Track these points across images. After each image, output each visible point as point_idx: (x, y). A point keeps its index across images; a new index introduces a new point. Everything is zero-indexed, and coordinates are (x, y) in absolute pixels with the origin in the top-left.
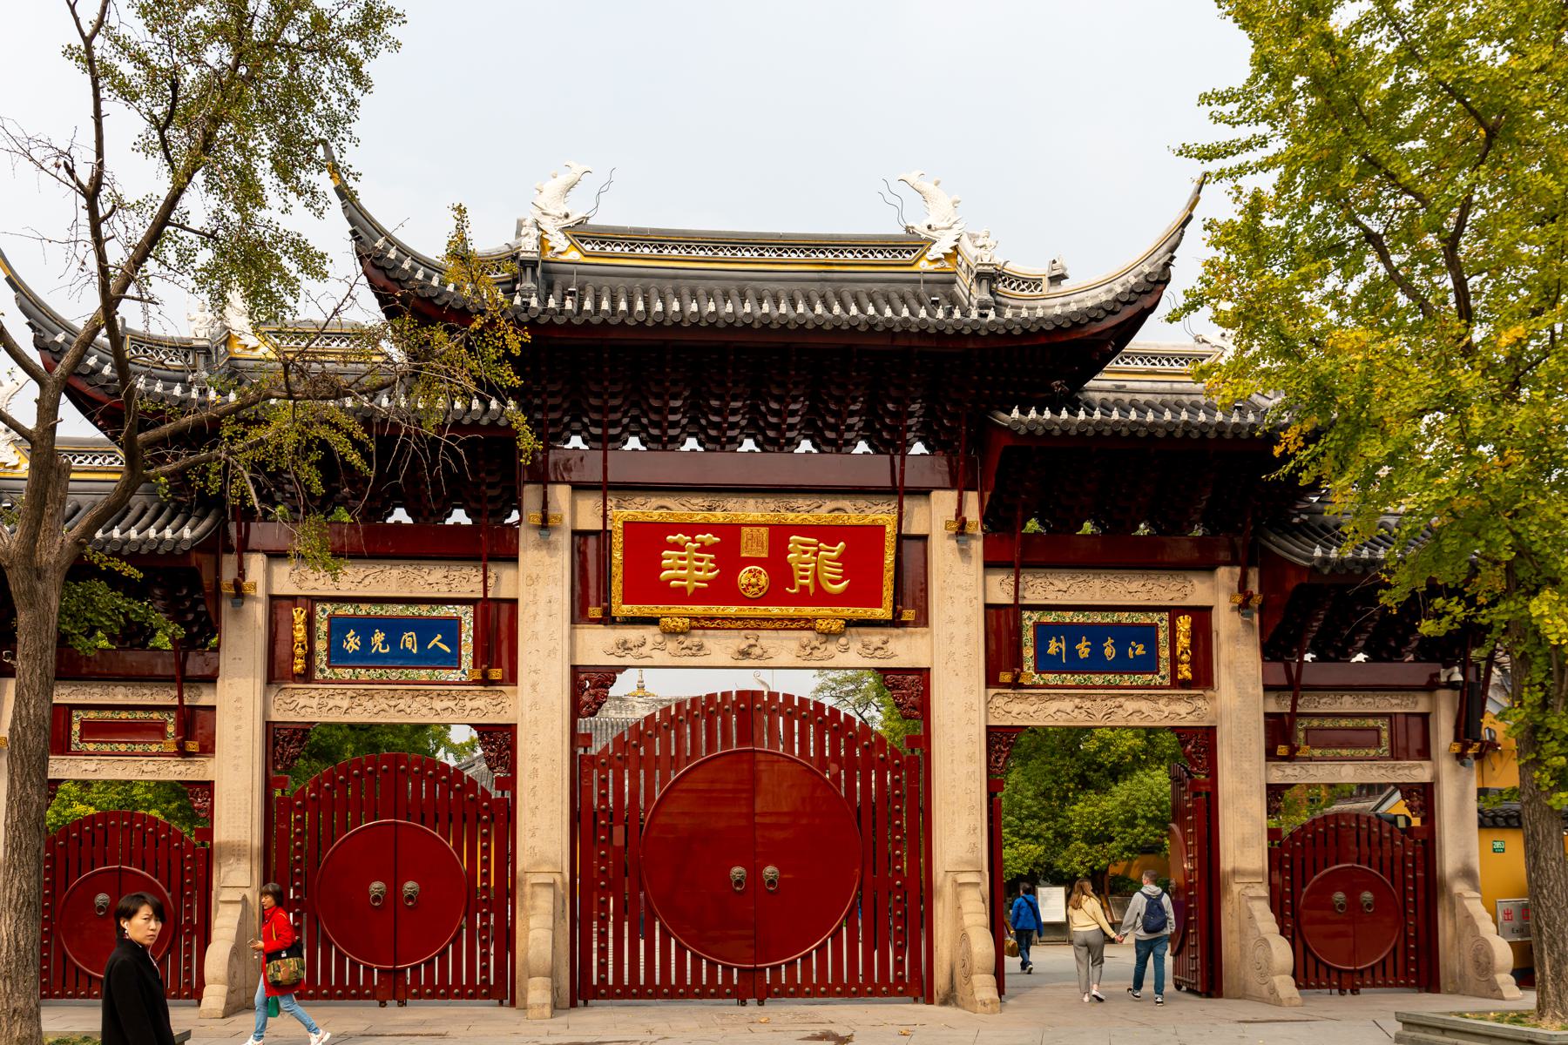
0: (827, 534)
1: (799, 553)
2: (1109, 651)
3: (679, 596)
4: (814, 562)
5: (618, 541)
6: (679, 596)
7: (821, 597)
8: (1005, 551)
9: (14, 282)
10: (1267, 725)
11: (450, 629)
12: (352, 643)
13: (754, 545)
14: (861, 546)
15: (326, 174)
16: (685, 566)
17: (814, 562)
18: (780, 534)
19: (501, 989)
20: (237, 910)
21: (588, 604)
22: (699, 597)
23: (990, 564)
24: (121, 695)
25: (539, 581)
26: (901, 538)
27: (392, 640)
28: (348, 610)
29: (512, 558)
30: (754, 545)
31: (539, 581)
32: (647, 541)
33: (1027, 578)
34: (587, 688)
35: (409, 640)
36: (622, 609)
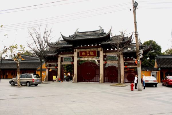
0: (92, 51)
1: (90, 52)
2: (111, 58)
3: (83, 56)
4: (91, 53)
5: (79, 53)
6: (83, 56)
7: (92, 55)
8: (46, 62)
9: (61, 34)
10: (61, 66)
11: (71, 58)
12: (65, 60)
13: (88, 52)
14: (94, 52)
15: (33, 53)
16: (84, 54)
17: (91, 53)
18: (89, 52)
19: (98, 81)
20: (101, 75)
21: (78, 56)
22: (85, 56)
23: (104, 52)
24: (131, 67)
25: (75, 55)
26: (97, 51)
27: (68, 59)
28: (109, 56)
29: (74, 54)
30: (88, 52)
31: (75, 55)
32: (81, 52)
33: (106, 53)
34: (78, 62)
35: (68, 59)
36: (80, 57)
